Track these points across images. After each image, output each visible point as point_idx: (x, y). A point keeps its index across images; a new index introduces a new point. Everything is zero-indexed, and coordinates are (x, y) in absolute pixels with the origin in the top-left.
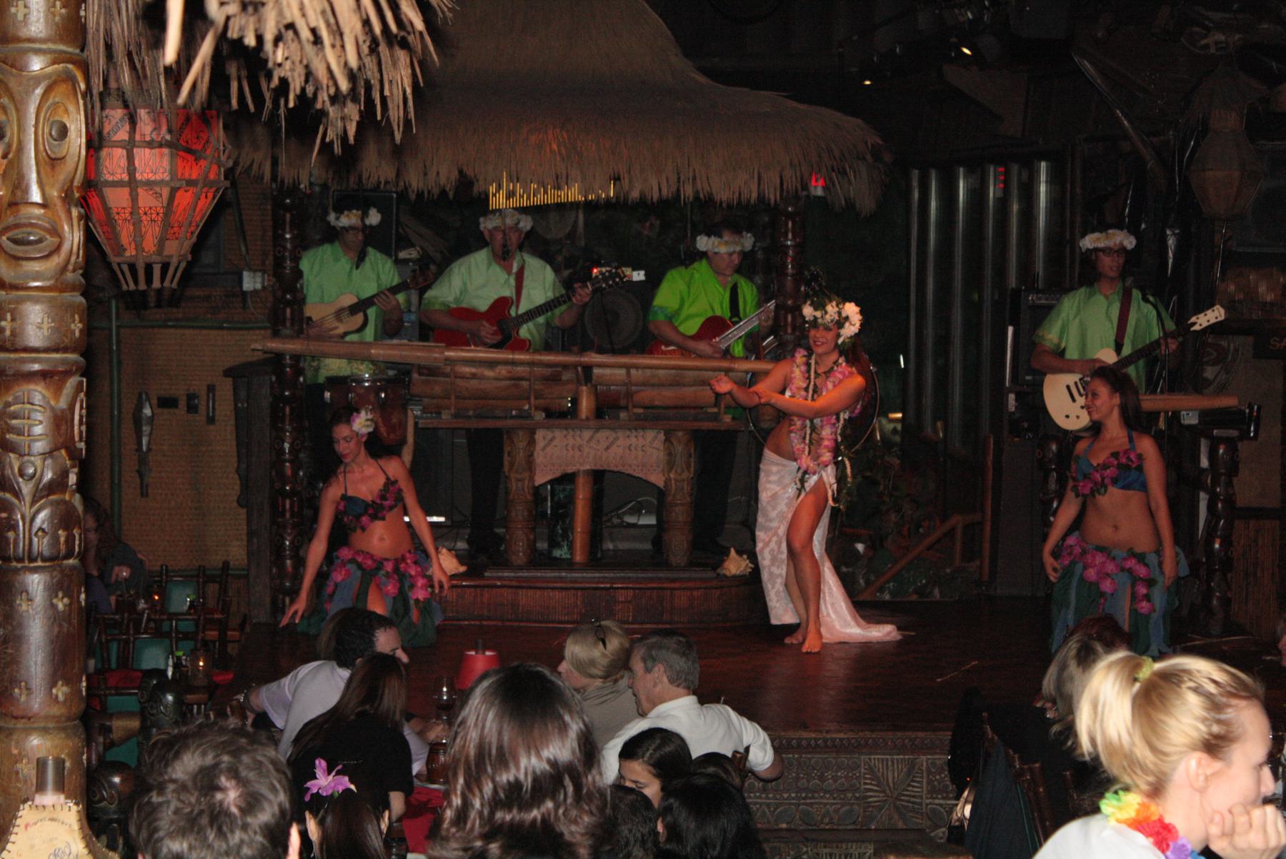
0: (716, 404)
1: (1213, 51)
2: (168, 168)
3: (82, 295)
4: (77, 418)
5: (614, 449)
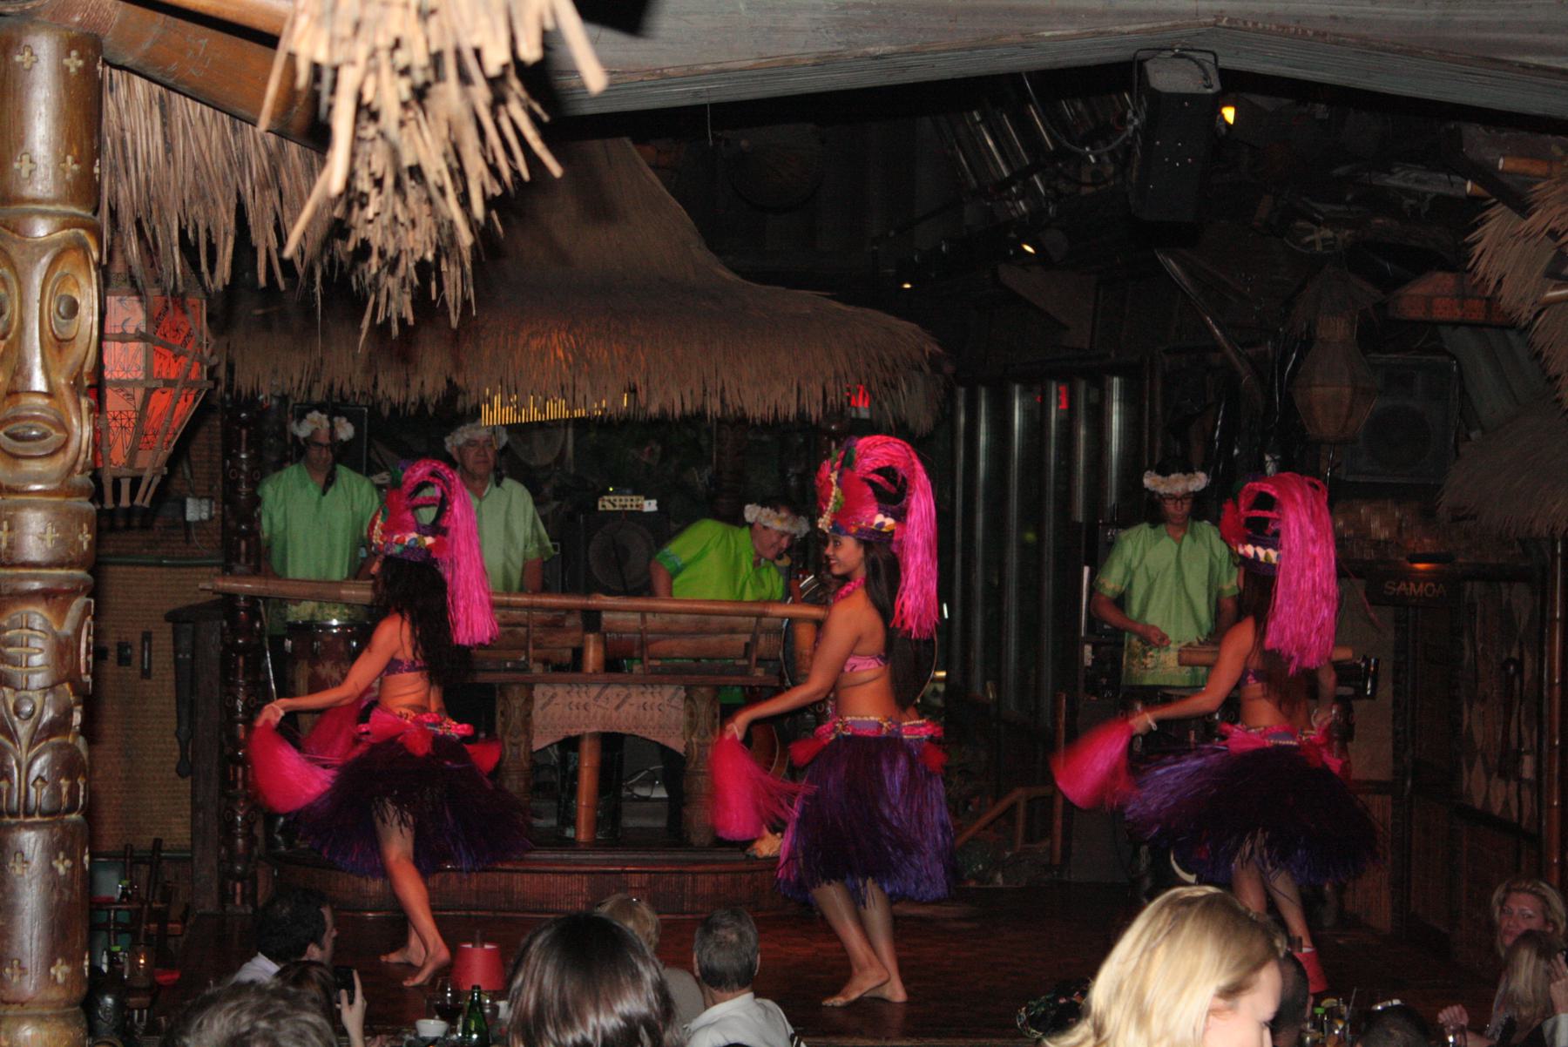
0: (746, 656)
1: (1319, 248)
2: (142, 365)
5: (626, 707)
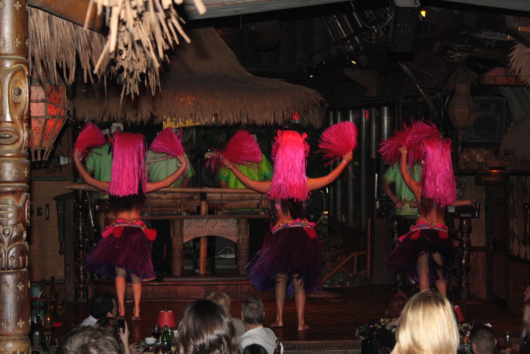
1: (456, 60)
2: (44, 111)
3: (28, 159)
4: (26, 210)
5: (216, 227)
